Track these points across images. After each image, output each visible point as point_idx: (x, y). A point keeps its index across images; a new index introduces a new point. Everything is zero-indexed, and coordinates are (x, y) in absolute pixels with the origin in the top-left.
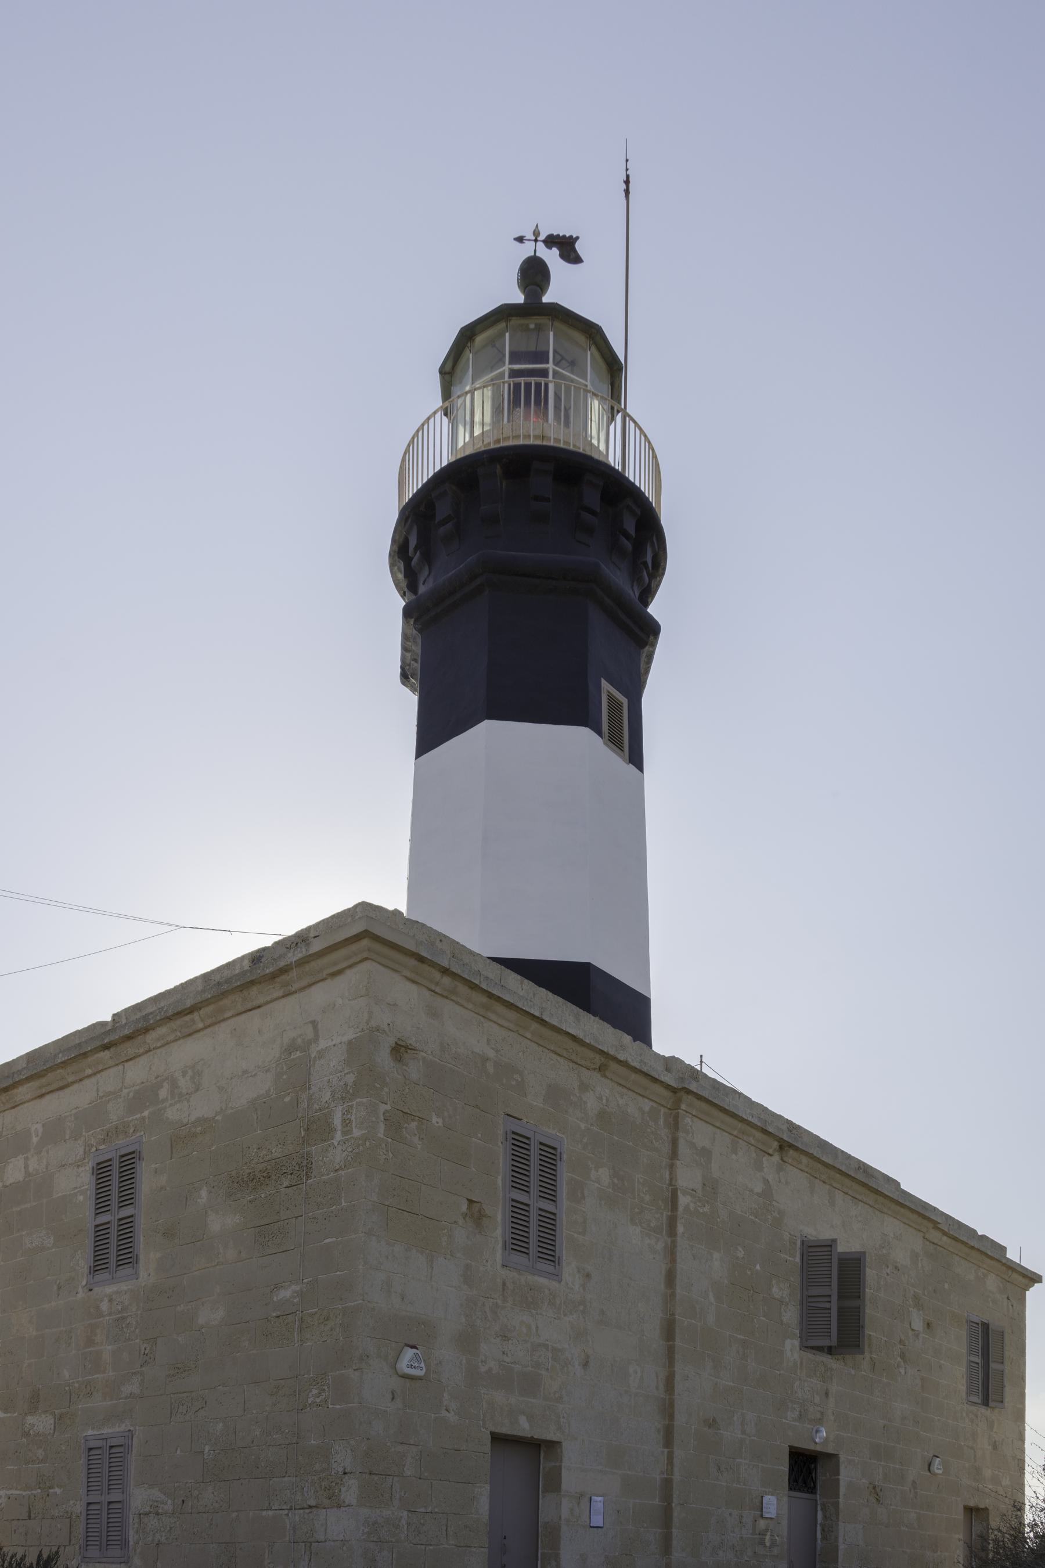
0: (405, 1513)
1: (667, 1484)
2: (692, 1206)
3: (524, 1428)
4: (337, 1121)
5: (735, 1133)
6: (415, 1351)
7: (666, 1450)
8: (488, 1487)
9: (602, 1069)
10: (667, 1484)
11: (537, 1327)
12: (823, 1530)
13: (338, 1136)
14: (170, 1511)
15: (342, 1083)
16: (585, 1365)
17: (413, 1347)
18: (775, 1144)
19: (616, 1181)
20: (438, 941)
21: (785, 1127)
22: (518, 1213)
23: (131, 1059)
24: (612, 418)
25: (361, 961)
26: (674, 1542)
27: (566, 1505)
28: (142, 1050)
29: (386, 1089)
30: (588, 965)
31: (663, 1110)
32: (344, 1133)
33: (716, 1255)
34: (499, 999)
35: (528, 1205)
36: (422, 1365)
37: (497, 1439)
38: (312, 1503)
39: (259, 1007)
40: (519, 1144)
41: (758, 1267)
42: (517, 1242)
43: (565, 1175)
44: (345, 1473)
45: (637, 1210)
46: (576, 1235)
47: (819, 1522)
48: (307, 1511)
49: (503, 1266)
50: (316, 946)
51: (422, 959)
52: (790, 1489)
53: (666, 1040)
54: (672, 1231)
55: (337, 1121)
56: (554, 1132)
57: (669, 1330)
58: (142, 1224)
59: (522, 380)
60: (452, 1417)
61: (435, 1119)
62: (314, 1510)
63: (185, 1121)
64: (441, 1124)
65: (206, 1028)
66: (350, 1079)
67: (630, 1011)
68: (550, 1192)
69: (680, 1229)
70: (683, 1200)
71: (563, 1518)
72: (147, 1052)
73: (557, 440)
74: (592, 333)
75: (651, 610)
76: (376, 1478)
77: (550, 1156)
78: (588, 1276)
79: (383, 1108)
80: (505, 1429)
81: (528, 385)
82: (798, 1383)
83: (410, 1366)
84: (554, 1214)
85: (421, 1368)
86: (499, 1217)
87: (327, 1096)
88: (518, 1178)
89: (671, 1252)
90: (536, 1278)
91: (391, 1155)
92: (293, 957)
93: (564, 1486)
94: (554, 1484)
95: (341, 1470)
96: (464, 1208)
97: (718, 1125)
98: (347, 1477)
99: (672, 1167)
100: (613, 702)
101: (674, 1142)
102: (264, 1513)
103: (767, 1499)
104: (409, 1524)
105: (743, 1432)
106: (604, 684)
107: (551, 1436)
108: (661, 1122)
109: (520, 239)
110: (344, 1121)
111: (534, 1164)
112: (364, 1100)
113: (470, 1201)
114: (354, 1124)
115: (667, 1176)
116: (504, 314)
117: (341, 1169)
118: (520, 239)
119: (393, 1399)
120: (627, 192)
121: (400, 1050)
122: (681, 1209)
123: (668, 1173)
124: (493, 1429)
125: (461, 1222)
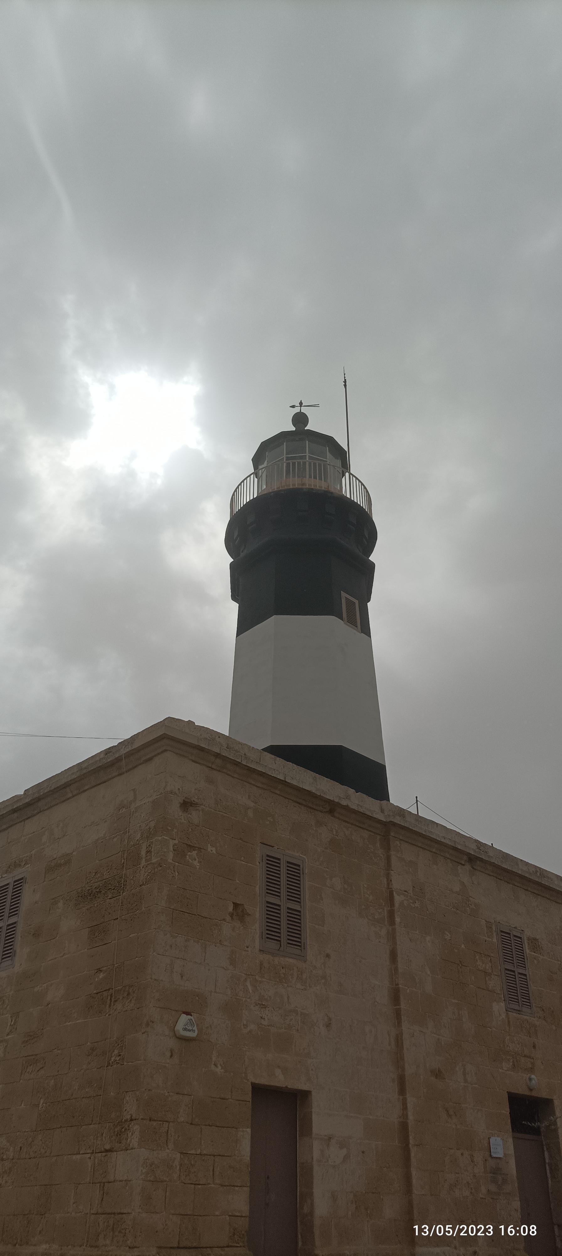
0: (178, 1155)
1: (404, 1126)
2: (405, 902)
3: (280, 1080)
4: (143, 853)
5: (434, 850)
6: (189, 1017)
7: (401, 1097)
8: (249, 1130)
9: (331, 812)
10: (404, 1126)
11: (288, 998)
12: (551, 1169)
13: (143, 862)
14: (11, 1157)
15: (148, 827)
16: (328, 1026)
17: (188, 1014)
18: (465, 857)
19: (346, 886)
20: (217, 737)
21: (473, 846)
22: (272, 910)
23: (29, 818)
24: (344, 475)
25: (162, 752)
26: (414, 1181)
27: (317, 1146)
28: (36, 812)
29: (175, 830)
30: (339, 750)
31: (378, 837)
32: (146, 861)
33: (428, 938)
34: (254, 771)
35: (279, 906)
36: (195, 1028)
37: (258, 1090)
38: (108, 1147)
39: (105, 782)
40: (272, 862)
41: (463, 946)
42: (271, 932)
43: (307, 884)
44: (131, 1120)
45: (363, 907)
46: (317, 927)
47: (547, 1161)
48: (104, 1154)
49: (260, 950)
50: (137, 745)
51: (202, 749)
52: (513, 1131)
53: (400, 794)
54: (392, 922)
55: (143, 853)
56: (297, 855)
57: (395, 996)
58: (20, 928)
59: (290, 461)
60: (219, 1070)
61: (210, 848)
62: (109, 1154)
63: (55, 857)
64: (214, 852)
65: (73, 796)
66: (152, 824)
67: (369, 776)
68: (295, 895)
69: (398, 920)
70: (397, 899)
71: (315, 1159)
72: (39, 813)
73: (294, 485)
74: (329, 442)
75: (371, 558)
76: (155, 1123)
77: (295, 871)
78: (328, 956)
79: (172, 843)
80: (264, 1080)
81: (315, 464)
82: (508, 1037)
83: (185, 1029)
84: (300, 912)
85: (194, 1031)
86: (257, 915)
87: (138, 836)
88: (272, 885)
89: (392, 936)
90: (287, 959)
91: (177, 874)
92: (123, 751)
93: (315, 1130)
94: (307, 1130)
95: (129, 1117)
96: (231, 908)
97: (420, 845)
98: (132, 1123)
99: (388, 876)
100: (350, 604)
101: (388, 859)
102: (74, 1157)
103: (492, 1140)
104: (181, 1165)
105: (466, 1081)
106: (343, 594)
107: (302, 1085)
108: (378, 845)
109: (293, 407)
110: (147, 852)
111: (284, 878)
112: (160, 838)
113: (236, 905)
114: (153, 854)
115: (386, 882)
116: (282, 437)
117: (143, 884)
118: (293, 407)
119: (171, 1056)
120: (345, 385)
121: (186, 805)
122: (397, 904)
123: (385, 880)
124: (254, 1081)
125: (228, 918)
